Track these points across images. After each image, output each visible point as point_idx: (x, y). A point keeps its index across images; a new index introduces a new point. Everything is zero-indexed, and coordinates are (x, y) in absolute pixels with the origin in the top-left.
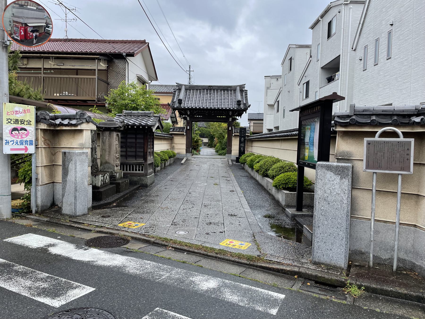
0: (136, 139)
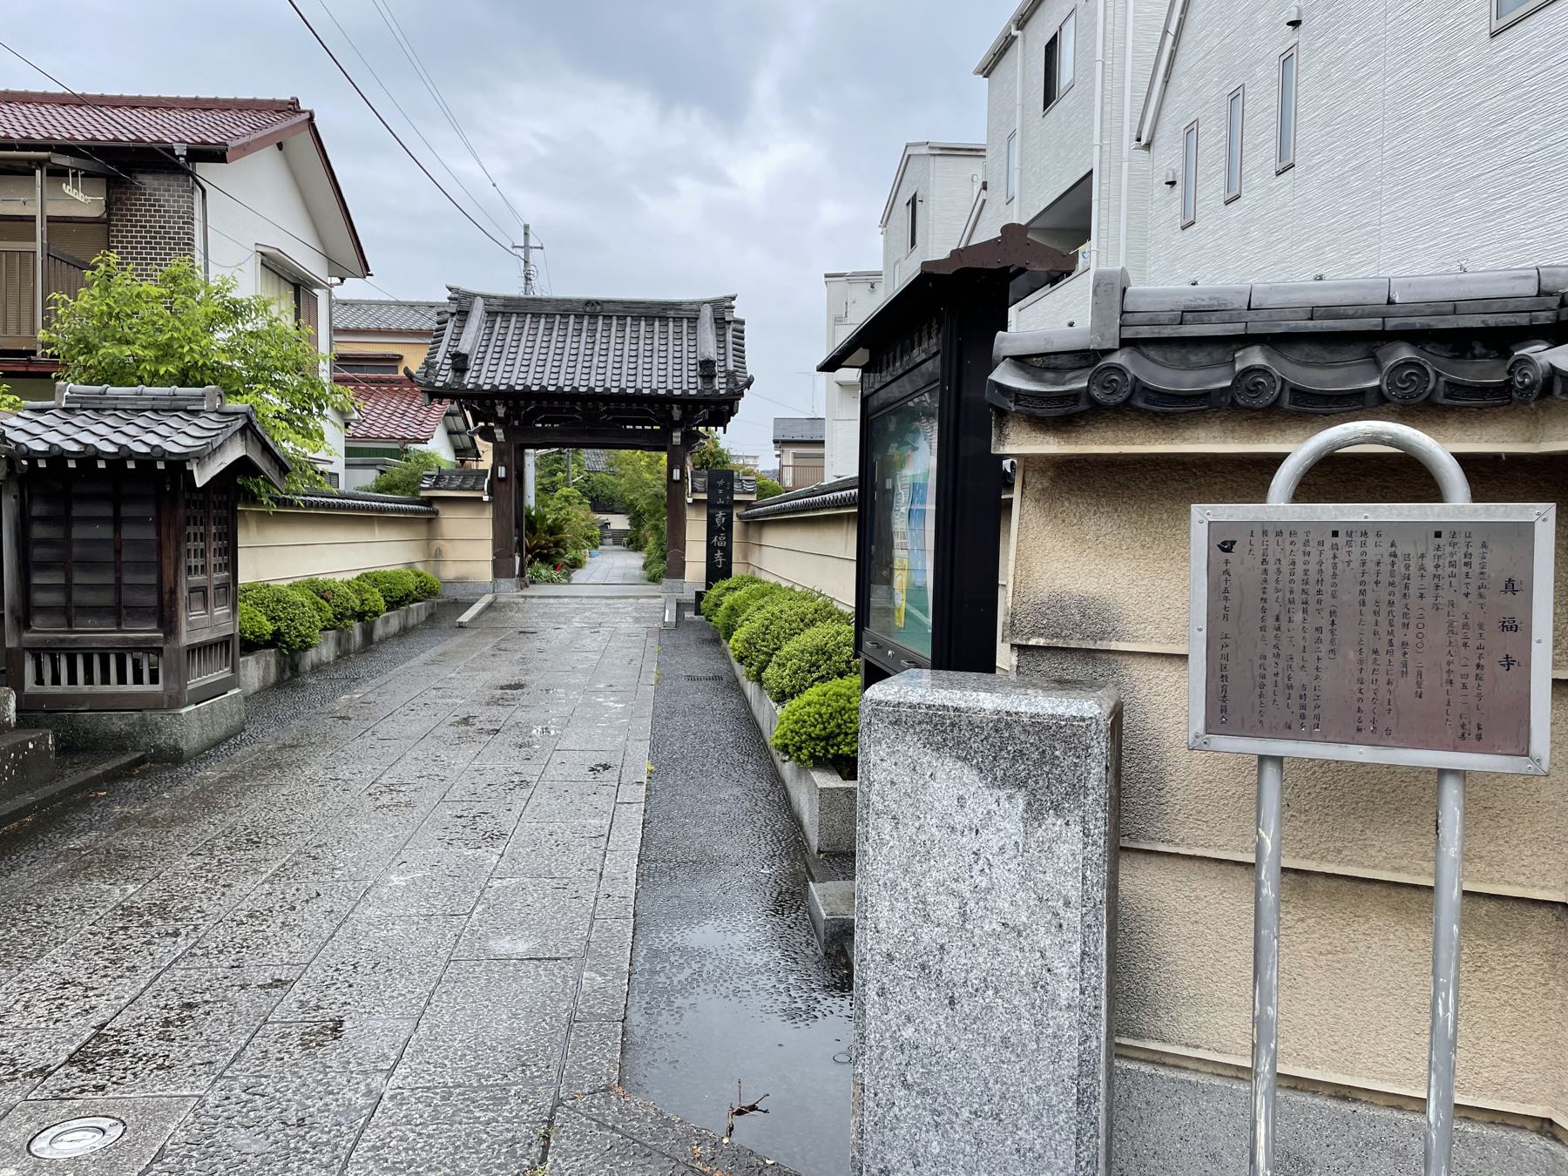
0: (117, 522)
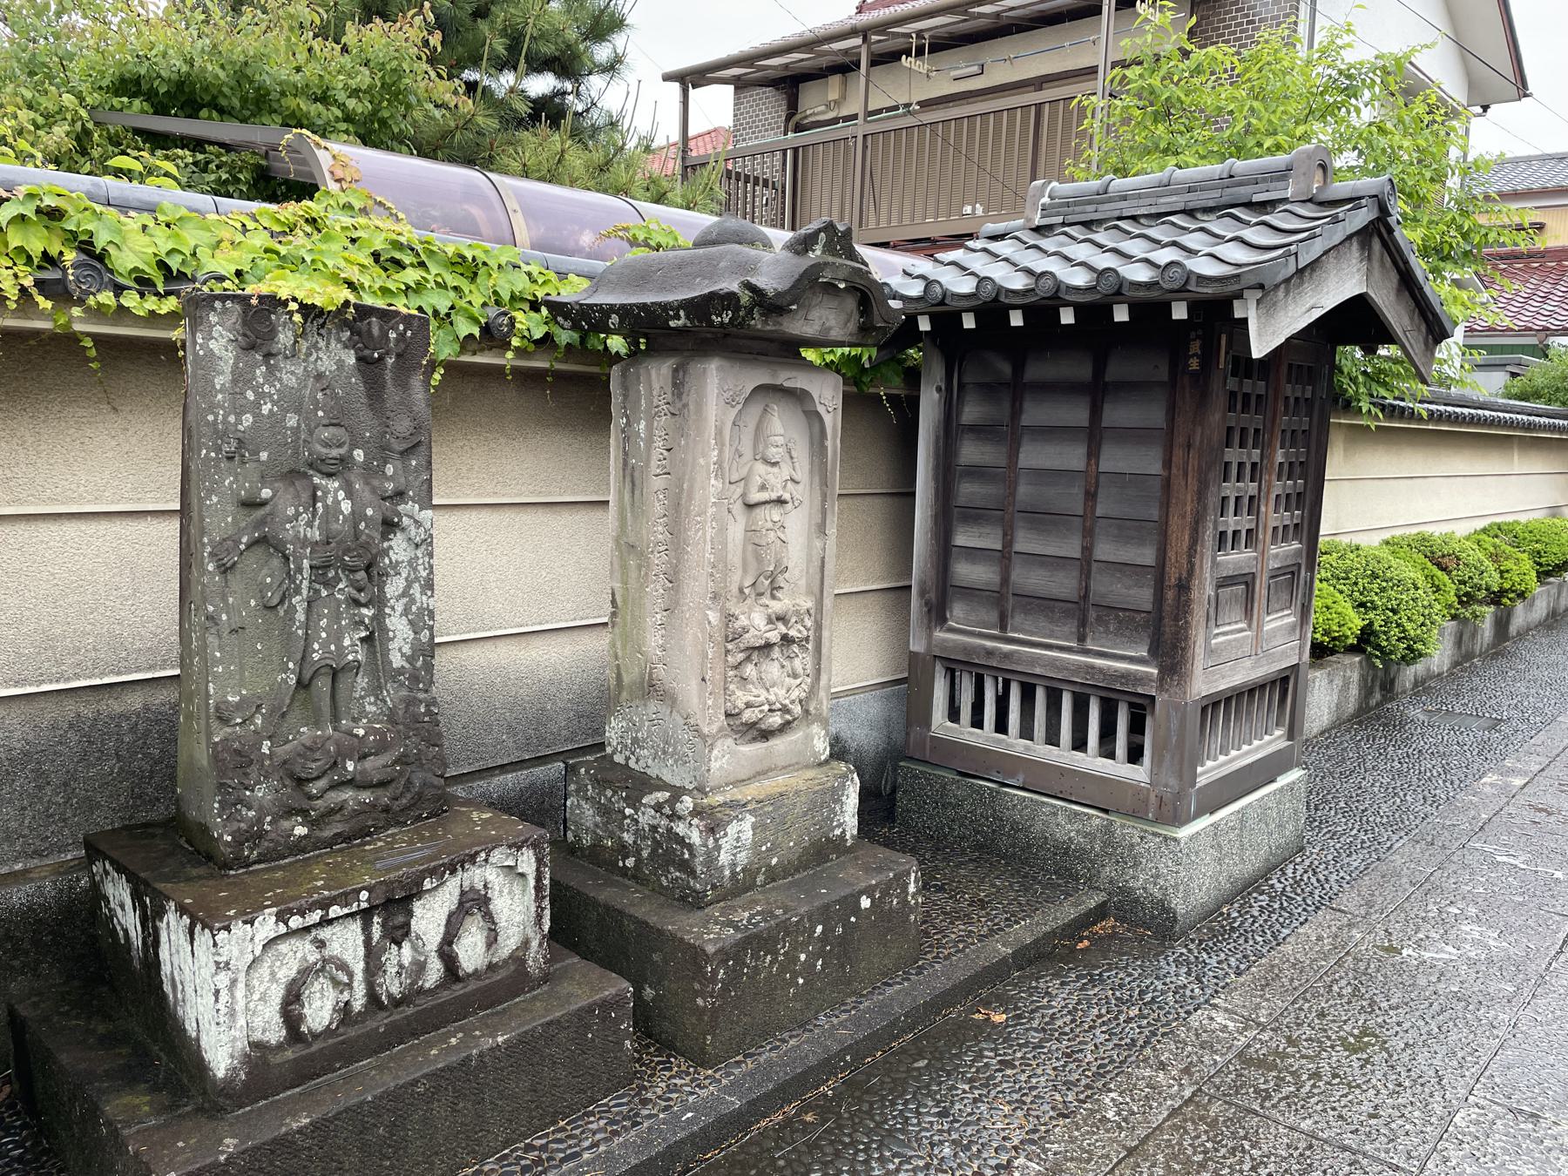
0: (1094, 437)
